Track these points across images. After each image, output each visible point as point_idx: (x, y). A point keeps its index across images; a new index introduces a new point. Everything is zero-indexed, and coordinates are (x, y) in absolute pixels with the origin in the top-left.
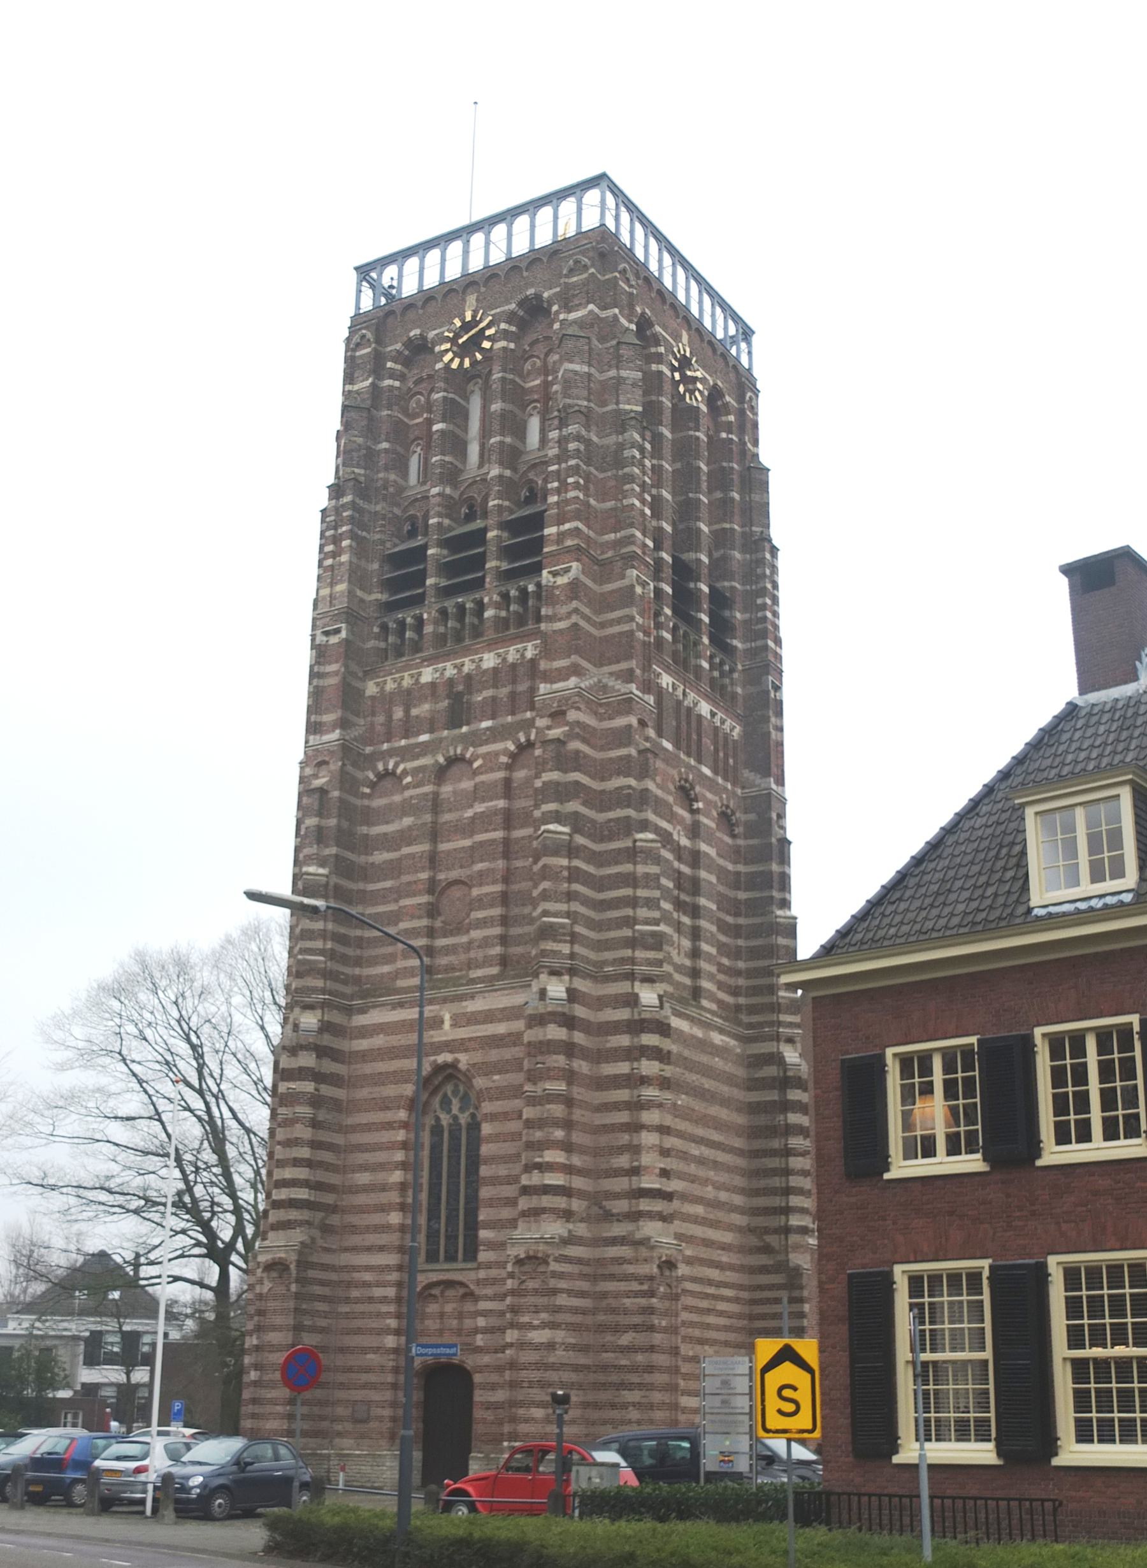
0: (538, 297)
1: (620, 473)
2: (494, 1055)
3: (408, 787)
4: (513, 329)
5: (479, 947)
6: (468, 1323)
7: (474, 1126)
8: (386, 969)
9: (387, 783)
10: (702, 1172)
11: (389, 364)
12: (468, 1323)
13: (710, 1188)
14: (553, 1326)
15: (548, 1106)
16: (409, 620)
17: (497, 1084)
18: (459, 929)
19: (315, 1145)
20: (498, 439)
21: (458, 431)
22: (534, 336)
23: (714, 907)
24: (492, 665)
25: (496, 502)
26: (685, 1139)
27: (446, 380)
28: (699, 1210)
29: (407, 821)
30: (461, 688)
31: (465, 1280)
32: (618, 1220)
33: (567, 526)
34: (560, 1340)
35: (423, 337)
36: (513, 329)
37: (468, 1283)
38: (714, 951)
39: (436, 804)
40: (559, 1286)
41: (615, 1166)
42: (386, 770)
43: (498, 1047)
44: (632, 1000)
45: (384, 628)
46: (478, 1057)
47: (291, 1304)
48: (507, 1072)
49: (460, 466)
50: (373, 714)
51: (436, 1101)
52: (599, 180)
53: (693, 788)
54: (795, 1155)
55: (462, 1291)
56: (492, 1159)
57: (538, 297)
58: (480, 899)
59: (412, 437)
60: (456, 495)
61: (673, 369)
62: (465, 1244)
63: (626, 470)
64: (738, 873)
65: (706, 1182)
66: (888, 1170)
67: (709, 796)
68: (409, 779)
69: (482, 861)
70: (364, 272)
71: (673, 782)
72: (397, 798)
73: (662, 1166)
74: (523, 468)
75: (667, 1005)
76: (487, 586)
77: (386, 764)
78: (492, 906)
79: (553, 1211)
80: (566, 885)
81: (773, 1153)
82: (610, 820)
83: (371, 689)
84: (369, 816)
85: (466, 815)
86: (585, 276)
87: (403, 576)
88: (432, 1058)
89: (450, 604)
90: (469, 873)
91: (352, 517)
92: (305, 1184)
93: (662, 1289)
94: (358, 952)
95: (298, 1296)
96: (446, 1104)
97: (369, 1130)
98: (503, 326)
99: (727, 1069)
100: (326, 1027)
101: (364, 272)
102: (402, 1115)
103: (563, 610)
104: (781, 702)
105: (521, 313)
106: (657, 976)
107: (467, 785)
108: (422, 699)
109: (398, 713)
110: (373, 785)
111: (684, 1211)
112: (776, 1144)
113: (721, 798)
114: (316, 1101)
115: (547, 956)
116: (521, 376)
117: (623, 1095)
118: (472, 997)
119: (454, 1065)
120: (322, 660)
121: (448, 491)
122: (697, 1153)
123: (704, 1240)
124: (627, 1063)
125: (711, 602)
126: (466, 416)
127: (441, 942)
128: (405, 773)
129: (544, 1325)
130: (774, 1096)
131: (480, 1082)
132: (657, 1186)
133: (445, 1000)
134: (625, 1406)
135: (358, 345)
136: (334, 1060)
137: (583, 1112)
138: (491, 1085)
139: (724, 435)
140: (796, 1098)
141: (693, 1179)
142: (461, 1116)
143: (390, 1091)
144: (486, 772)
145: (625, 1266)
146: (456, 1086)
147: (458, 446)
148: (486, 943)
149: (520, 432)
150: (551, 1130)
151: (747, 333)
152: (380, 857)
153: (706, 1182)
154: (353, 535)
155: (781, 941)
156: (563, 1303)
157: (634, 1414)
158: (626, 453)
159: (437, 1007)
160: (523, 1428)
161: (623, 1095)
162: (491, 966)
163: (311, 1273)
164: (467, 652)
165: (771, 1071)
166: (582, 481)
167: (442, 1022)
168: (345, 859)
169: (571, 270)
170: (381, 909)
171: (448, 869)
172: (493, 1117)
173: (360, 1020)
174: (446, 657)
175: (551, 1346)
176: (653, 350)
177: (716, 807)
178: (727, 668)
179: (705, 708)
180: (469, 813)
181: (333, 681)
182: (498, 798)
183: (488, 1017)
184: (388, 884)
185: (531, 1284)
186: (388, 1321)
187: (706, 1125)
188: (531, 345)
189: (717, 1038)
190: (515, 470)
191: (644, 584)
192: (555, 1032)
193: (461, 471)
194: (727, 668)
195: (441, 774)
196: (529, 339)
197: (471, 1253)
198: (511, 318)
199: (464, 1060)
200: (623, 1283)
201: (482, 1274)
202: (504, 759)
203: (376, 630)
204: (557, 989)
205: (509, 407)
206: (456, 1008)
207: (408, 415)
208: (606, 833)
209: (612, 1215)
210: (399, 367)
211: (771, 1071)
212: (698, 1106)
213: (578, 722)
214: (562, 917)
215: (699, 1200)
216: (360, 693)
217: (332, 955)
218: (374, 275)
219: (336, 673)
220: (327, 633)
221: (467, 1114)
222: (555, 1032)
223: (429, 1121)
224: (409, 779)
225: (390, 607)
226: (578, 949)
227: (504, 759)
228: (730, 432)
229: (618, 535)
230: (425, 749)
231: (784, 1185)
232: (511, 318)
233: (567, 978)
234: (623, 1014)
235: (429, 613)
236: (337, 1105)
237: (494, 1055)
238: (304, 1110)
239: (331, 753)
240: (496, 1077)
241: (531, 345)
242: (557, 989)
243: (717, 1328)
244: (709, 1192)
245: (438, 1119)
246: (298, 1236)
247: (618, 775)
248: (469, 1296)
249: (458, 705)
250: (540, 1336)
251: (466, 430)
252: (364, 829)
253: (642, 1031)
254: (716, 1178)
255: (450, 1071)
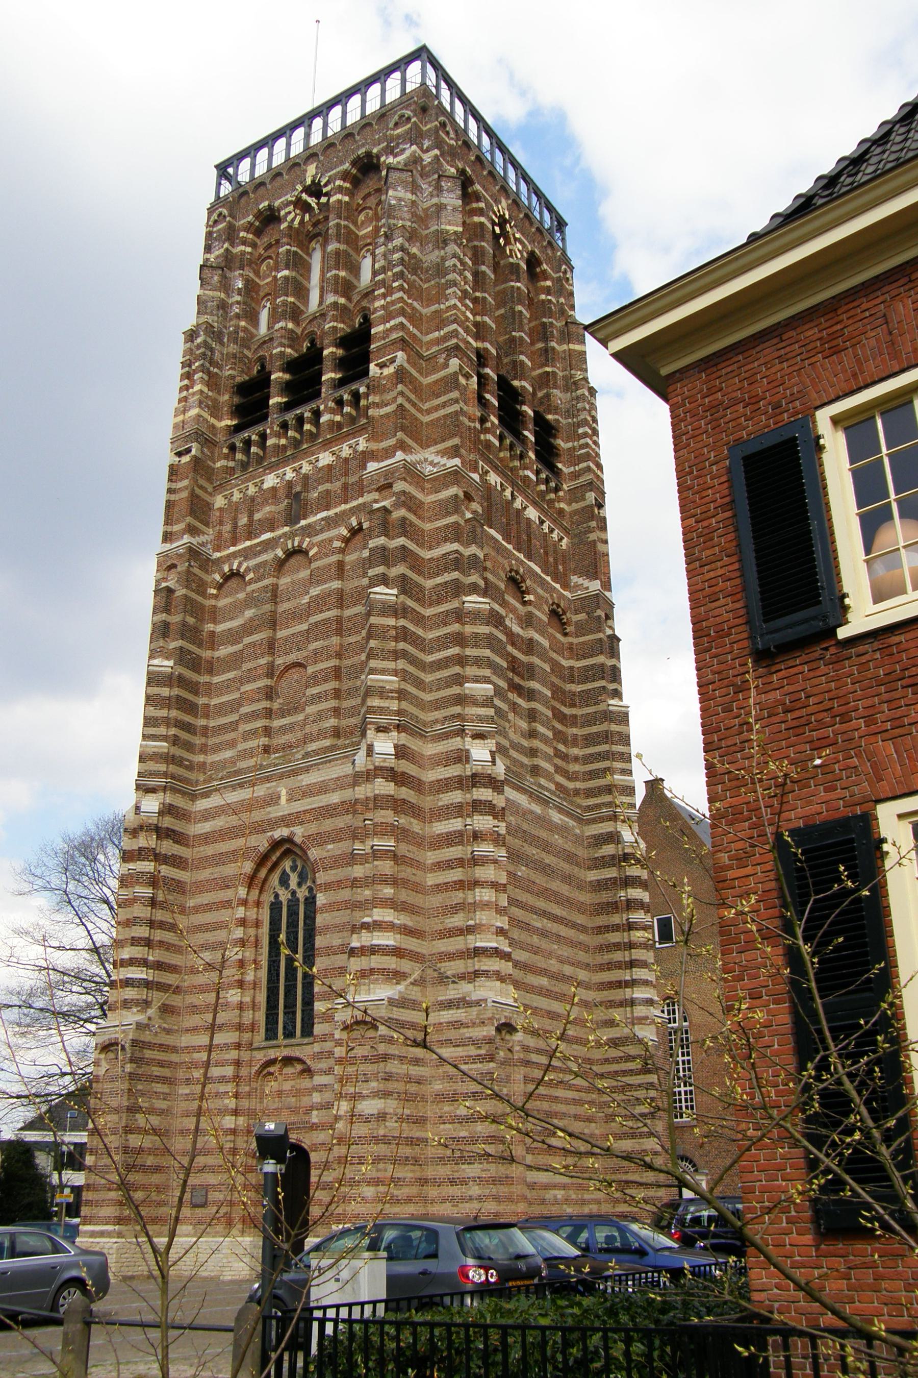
0: (368, 154)
1: (443, 281)
2: (328, 825)
3: (251, 582)
4: (348, 185)
5: (314, 721)
6: (306, 1101)
7: (311, 901)
8: (228, 754)
9: (233, 583)
10: (544, 944)
11: (242, 234)
12: (306, 1101)
13: (553, 962)
14: (386, 1094)
15: (376, 863)
16: (254, 437)
17: (330, 854)
18: (296, 709)
19: (152, 924)
20: (334, 272)
21: (300, 278)
22: (366, 191)
23: (549, 694)
24: (326, 463)
25: (331, 324)
26: (527, 910)
27: (290, 237)
28: (544, 981)
29: (249, 613)
30: (298, 489)
31: (301, 1056)
32: (454, 982)
33: (392, 323)
34: (391, 1111)
35: (270, 208)
36: (348, 185)
37: (305, 1058)
38: (550, 734)
39: (274, 594)
40: (390, 1052)
41: (450, 925)
42: (231, 570)
43: (331, 816)
44: (462, 757)
45: (232, 448)
46: (313, 828)
47: (126, 1086)
48: (341, 840)
49: (302, 308)
50: (221, 523)
51: (275, 879)
52: (422, 54)
53: (524, 581)
54: (637, 929)
55: (299, 1067)
56: (327, 929)
57: (368, 154)
58: (314, 676)
59: (262, 294)
60: (299, 331)
61: (494, 223)
62: (303, 1020)
63: (448, 277)
64: (571, 668)
65: (549, 955)
66: (844, 622)
67: (539, 591)
68: (251, 575)
69: (316, 640)
70: (223, 170)
71: (504, 569)
72: (241, 596)
73: (499, 924)
74: (356, 298)
75: (498, 760)
76: (323, 395)
77: (231, 565)
78: (326, 681)
79: (383, 971)
80: (393, 644)
81: (616, 928)
82: (438, 585)
83: (219, 501)
84: (214, 615)
85: (304, 602)
86: (409, 126)
87: (250, 403)
88: (269, 834)
89: (290, 416)
90: (305, 654)
91: (204, 354)
92: (144, 963)
93: (502, 1053)
94: (203, 740)
95: (132, 1076)
96: (284, 881)
97: (210, 910)
98: (338, 183)
99: (566, 847)
100: (167, 810)
101: (223, 170)
102: (242, 892)
103: (389, 396)
104: (605, 518)
105: (354, 171)
106: (489, 732)
107: (304, 574)
108: (265, 502)
109: (243, 520)
110: (220, 587)
111: (525, 981)
112: (616, 919)
113: (552, 596)
114: (153, 881)
115: (374, 713)
116: (355, 223)
117: (455, 852)
118: (307, 770)
119: (289, 840)
120: (174, 478)
121: (290, 325)
122: (539, 925)
123: (549, 1012)
124: (459, 819)
125: (535, 425)
126: (308, 268)
127: (277, 723)
128: (248, 570)
129: (376, 1094)
130: (612, 873)
131: (314, 853)
132: (494, 945)
133: (281, 777)
134: (464, 1182)
135: (216, 222)
136: (176, 842)
137: (414, 871)
138: (325, 854)
139: (543, 297)
140: (636, 874)
141: (536, 951)
142: (298, 891)
143: (230, 870)
144: (321, 558)
145: (463, 1031)
146: (294, 861)
147: (302, 292)
148: (320, 716)
149: (355, 269)
150: (379, 887)
151: (561, 224)
152: (223, 651)
153: (549, 955)
154: (203, 369)
155: (614, 727)
156: (394, 1070)
157: (475, 1190)
158: (447, 264)
159: (274, 784)
160: (353, 1208)
161: (455, 852)
162: (325, 738)
163: (148, 1054)
164: (306, 454)
165: (609, 850)
166: (406, 286)
167: (279, 798)
168: (190, 652)
169: (396, 124)
170: (224, 699)
171: (286, 654)
172: (328, 886)
173: (202, 804)
174: (285, 462)
175: (382, 1117)
176: (474, 205)
177: (546, 602)
178: (553, 484)
179: (532, 513)
180: (306, 599)
181: (184, 494)
182: (330, 579)
183: (322, 788)
184: (231, 675)
185: (359, 1052)
186: (227, 1101)
187: (548, 899)
188: (364, 199)
189: (556, 817)
190: (349, 299)
191: (467, 376)
192: (383, 787)
193: (302, 312)
194: (553, 484)
195: (280, 565)
196: (364, 191)
197: (308, 1030)
198: (345, 176)
199: (299, 833)
200: (460, 1049)
201: (317, 1048)
202: (337, 544)
203: (225, 451)
204: (384, 745)
205: (343, 247)
206: (292, 782)
207: (259, 276)
208: (435, 597)
209: (447, 977)
210: (250, 236)
211: (609, 850)
212: (540, 880)
213: (404, 492)
214: (389, 675)
215: (543, 972)
216: (209, 506)
217: (175, 741)
218: (231, 170)
219: (186, 488)
220: (179, 454)
221: (304, 887)
222: (383, 787)
223: (268, 898)
224: (251, 575)
225: (237, 429)
226: (404, 705)
227: (337, 544)
228: (548, 294)
229: (442, 333)
230: (268, 545)
231: (627, 959)
232: (345, 176)
233: (395, 734)
234: (454, 771)
235: (272, 428)
236: (178, 887)
237: (328, 825)
238: (146, 891)
239: (180, 556)
240: (330, 847)
241: (364, 199)
242: (384, 745)
243: (567, 1102)
244: (553, 965)
245: (277, 896)
246: (133, 1017)
247: (445, 542)
248: (308, 1071)
249: (296, 503)
250: (369, 1107)
251: (308, 279)
252: (210, 627)
253: (474, 786)
254: (560, 952)
255: (287, 846)
